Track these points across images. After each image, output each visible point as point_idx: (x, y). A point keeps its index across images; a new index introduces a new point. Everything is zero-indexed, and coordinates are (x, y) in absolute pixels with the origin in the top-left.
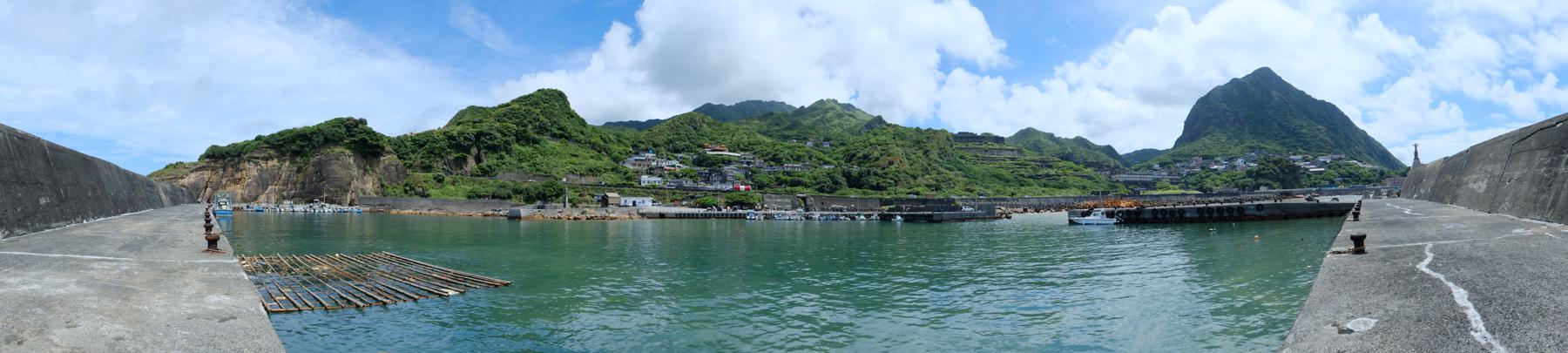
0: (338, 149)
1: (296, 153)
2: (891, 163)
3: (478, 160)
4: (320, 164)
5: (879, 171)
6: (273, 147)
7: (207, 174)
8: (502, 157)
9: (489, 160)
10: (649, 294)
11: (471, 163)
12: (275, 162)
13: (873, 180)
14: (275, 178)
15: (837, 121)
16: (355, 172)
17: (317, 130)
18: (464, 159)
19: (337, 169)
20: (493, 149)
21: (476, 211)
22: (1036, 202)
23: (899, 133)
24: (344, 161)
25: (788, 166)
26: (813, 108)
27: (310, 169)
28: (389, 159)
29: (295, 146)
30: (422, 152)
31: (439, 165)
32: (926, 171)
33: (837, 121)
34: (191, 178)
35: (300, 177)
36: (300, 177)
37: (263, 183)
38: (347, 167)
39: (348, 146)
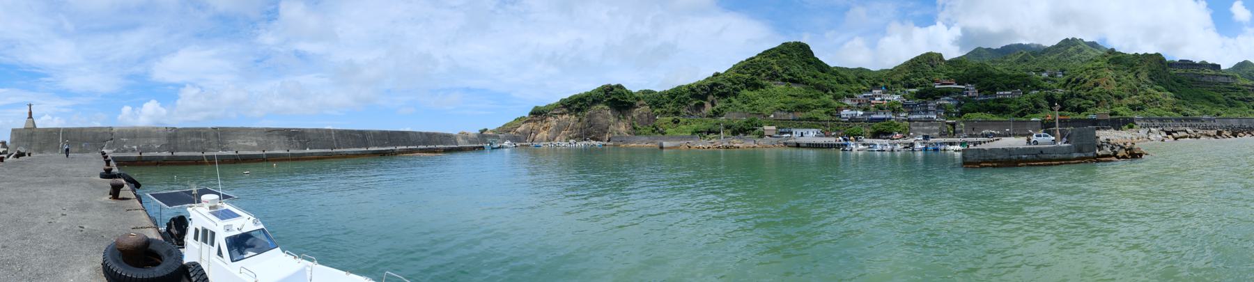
0: (600, 106)
1: (578, 110)
2: (1096, 85)
3: (713, 105)
4: (590, 116)
5: (1083, 93)
6: (565, 107)
7: (531, 125)
8: (730, 101)
9: (720, 104)
10: (943, 209)
11: (708, 108)
12: (567, 116)
13: (1075, 103)
14: (566, 126)
15: (1077, 55)
16: (612, 120)
17: (588, 95)
18: (703, 105)
19: (599, 119)
20: (724, 95)
21: (702, 143)
22: (1235, 123)
23: (1117, 59)
24: (604, 113)
25: (1000, 94)
26: (1059, 45)
27: (585, 119)
28: (642, 110)
29: (576, 105)
30: (674, 101)
31: (684, 111)
32: (1134, 91)
33: (1077, 55)
34: (522, 128)
35: (579, 125)
36: (579, 125)
37: (559, 129)
38: (606, 117)
39: (606, 104)
